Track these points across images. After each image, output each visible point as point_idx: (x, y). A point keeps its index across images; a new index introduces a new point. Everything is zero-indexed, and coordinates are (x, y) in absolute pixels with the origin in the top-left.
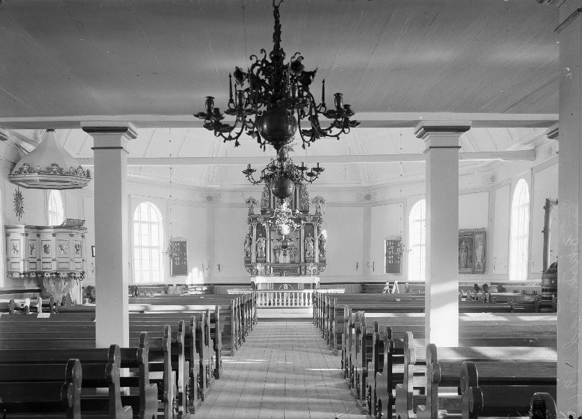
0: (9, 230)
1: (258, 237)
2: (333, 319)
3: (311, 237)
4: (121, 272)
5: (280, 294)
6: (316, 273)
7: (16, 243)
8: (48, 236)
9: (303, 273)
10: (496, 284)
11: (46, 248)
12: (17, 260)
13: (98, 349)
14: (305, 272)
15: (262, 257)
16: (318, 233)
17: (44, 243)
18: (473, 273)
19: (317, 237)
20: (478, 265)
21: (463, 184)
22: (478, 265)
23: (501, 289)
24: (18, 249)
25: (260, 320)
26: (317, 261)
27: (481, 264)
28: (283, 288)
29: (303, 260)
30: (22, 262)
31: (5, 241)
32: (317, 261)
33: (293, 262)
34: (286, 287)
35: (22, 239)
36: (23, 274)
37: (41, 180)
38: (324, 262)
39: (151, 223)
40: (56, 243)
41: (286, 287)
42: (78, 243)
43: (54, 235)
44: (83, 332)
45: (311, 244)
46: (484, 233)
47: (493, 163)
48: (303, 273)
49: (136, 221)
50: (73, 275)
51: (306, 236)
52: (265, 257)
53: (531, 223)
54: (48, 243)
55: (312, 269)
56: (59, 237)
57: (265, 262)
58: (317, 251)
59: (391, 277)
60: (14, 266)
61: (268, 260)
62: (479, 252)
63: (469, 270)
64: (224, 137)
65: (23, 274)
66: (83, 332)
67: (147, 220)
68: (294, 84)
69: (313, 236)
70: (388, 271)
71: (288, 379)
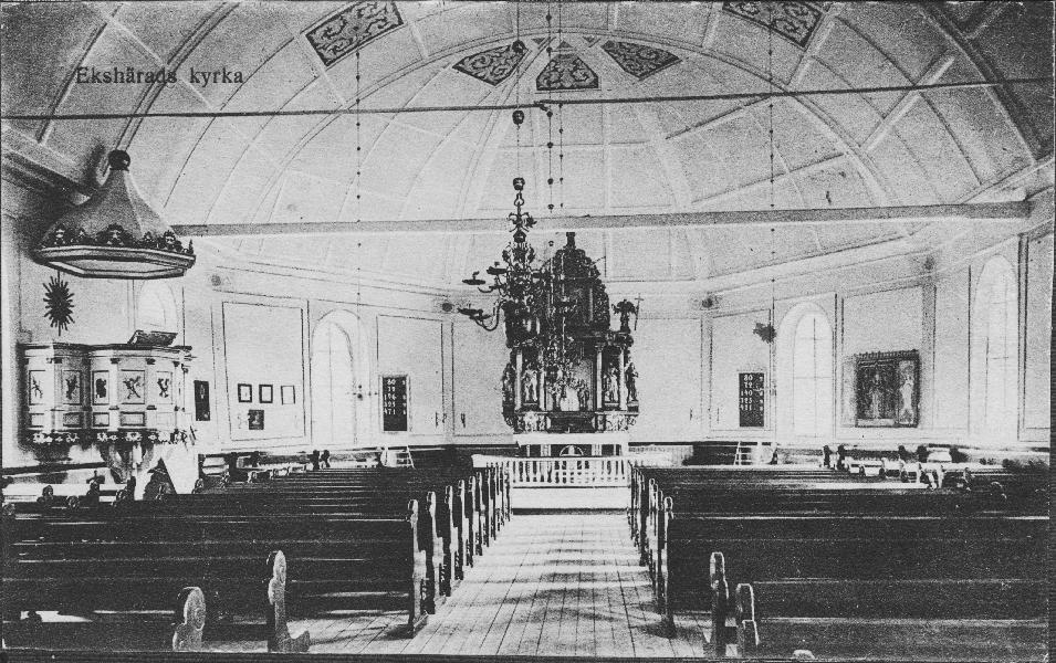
1: (524, 368)
2: (645, 510)
8: (102, 361)
9: (601, 427)
10: (948, 446)
11: (101, 386)
14: (604, 426)
15: (531, 401)
16: (626, 362)
18: (898, 426)
19: (623, 369)
21: (632, 656)
23: (957, 456)
25: (518, 512)
26: (624, 406)
27: (911, 412)
28: (566, 451)
30: (48, 414)
32: (624, 406)
34: (572, 451)
36: (51, 435)
38: (636, 409)
40: (119, 377)
41: (572, 451)
42: (165, 376)
45: (614, 378)
46: (913, 356)
50: (152, 437)
53: (715, 443)
55: (615, 422)
56: (124, 364)
58: (624, 390)
59: (750, 434)
61: (542, 406)
62: (906, 391)
65: (51, 435)
68: (892, 589)
70: (743, 424)
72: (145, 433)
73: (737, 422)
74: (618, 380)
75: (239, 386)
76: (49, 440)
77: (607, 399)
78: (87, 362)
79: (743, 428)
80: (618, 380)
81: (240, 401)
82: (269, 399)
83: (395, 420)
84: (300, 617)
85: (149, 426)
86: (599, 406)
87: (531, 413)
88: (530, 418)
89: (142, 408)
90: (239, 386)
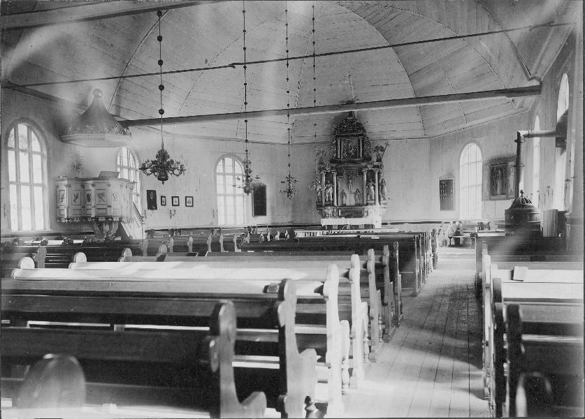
3: (372, 183)
4: (268, 369)
11: (89, 196)
13: (216, 199)
15: (329, 200)
20: (511, 191)
22: (511, 191)
24: (97, 196)
40: (95, 192)
43: (93, 185)
44: (508, 388)
45: (372, 188)
47: (309, 116)
51: (368, 181)
52: (333, 201)
54: (89, 192)
57: (333, 205)
60: (89, 212)
63: (504, 196)
64: (480, 269)
66: (508, 388)
69: (374, 181)
70: (265, 215)
72: (107, 218)
73: (294, 321)
74: (374, 189)
75: (173, 197)
76: (67, 221)
77: (369, 199)
78: (83, 186)
79: (456, 206)
80: (374, 189)
81: (179, 205)
82: (191, 205)
83: (260, 209)
84: (273, 343)
85: (109, 214)
86: (365, 203)
87: (330, 208)
88: (329, 210)
89: (105, 207)
90: (173, 197)
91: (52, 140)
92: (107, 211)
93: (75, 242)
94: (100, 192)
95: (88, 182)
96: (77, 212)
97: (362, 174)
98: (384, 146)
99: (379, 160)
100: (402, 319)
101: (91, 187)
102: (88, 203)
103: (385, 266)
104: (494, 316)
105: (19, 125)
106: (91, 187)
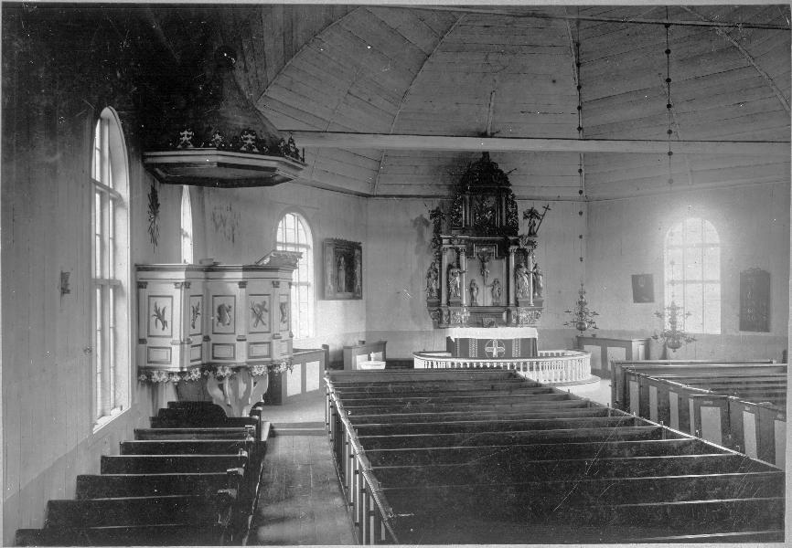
0: (144, 274)
5: (528, 363)
6: (531, 323)
7: (162, 303)
9: (514, 321)
12: (167, 342)
17: (219, 301)
24: (167, 317)
29: (512, 302)
31: (134, 297)
33: (495, 305)
35: (178, 294)
37: (220, 165)
39: (702, 282)
43: (242, 285)
45: (526, 281)
48: (514, 321)
49: (280, 243)
51: (518, 267)
54: (228, 302)
67: (698, 278)
71: (248, 354)
89: (266, 338)
91: (160, 388)
92: (270, 350)
93: (250, 518)
94: (258, 300)
95: (228, 275)
96: (196, 353)
97: (508, 255)
98: (541, 211)
99: (532, 234)
100: (376, 346)
101: (234, 288)
102: (220, 328)
103: (290, 262)
104: (6, 101)
105: (288, 395)
106: (234, 288)
